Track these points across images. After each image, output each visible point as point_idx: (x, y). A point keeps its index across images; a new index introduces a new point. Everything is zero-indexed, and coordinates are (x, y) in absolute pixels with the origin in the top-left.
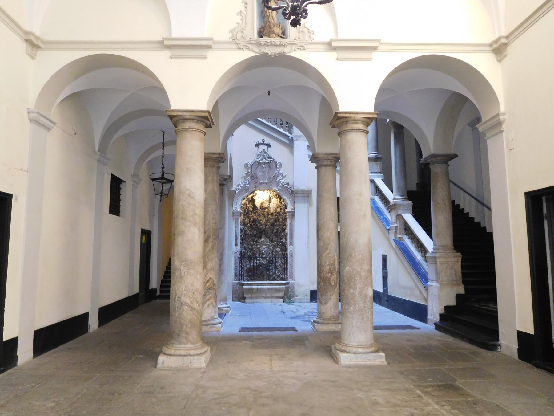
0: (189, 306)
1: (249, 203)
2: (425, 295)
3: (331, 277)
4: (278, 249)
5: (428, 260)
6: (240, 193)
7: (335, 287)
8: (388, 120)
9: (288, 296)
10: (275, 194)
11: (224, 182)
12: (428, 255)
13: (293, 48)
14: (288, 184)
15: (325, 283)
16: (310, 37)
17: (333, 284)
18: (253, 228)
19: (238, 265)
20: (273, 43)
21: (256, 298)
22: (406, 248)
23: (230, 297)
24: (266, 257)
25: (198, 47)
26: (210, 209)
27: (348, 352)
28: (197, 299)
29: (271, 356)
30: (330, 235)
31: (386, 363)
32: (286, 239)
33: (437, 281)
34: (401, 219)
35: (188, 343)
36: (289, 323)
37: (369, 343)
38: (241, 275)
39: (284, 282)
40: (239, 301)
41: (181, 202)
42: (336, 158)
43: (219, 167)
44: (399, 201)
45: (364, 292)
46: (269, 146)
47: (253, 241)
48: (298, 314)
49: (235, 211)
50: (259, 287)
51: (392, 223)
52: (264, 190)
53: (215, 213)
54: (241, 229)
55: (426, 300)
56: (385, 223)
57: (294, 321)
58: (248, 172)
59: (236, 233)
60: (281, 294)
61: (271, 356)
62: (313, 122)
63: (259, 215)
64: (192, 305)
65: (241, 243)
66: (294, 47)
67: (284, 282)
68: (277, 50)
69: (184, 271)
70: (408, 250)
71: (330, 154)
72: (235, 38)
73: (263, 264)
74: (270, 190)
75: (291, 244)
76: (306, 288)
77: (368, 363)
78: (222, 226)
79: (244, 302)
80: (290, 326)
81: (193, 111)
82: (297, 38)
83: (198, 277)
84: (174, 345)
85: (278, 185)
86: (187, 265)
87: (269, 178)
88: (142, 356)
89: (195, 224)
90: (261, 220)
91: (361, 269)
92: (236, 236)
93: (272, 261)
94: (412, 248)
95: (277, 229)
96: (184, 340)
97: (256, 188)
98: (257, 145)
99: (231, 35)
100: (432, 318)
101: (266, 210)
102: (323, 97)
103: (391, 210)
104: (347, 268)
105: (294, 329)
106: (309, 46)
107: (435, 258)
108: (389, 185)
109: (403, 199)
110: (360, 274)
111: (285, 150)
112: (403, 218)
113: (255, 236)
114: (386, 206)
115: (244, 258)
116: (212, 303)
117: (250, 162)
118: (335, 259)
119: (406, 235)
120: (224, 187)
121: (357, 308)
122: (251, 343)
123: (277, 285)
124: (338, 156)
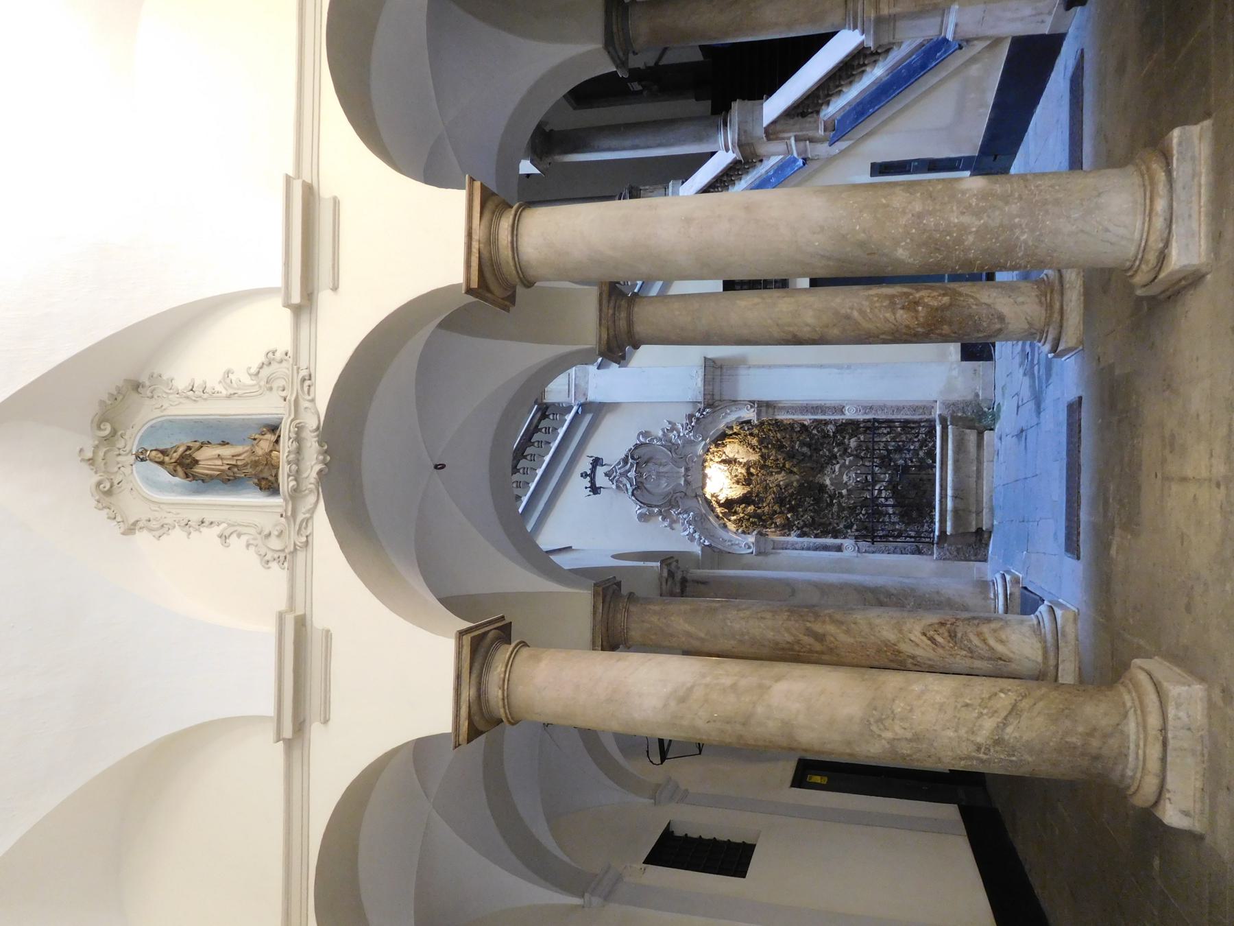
0: (1005, 723)
1: (736, 513)
2: (980, 46)
3: (926, 305)
4: (853, 443)
5: (885, 40)
6: (710, 536)
7: (955, 294)
8: (526, 167)
9: (976, 419)
10: (713, 449)
11: (679, 579)
12: (870, 44)
13: (307, 404)
14: (690, 417)
15: (943, 321)
16: (281, 362)
17: (946, 299)
18: (799, 505)
19: (891, 546)
20: (292, 457)
21: (979, 502)
22: (854, 109)
23: (975, 568)
24: (873, 474)
25: (309, 216)
26: (737, 626)
27: (1167, 244)
28: (986, 695)
29: (1167, 479)
30: (807, 307)
31: (1207, 123)
32: (826, 423)
33: (943, 11)
34: (779, 127)
35: (1122, 732)
36: (1054, 421)
37: (1137, 180)
38: (918, 537)
39: (938, 428)
40: (987, 545)
41: (700, 723)
42: (610, 296)
43: (631, 595)
44: (731, 135)
45: (974, 201)
46: (597, 462)
47: (832, 504)
48: (1026, 393)
49: (753, 549)
50: (950, 492)
51: (789, 151)
52: (705, 476)
53: (748, 613)
54: (799, 536)
55: (996, 41)
56: (789, 171)
57: (1048, 402)
58: (660, 513)
59: (808, 549)
60: (972, 436)
61: (1167, 479)
62: (518, 357)
63: (766, 488)
64: (1004, 714)
65: (836, 537)
66: (304, 404)
67: (938, 428)
68: (312, 448)
69: (898, 729)
70: (858, 104)
71: (601, 310)
72: (282, 555)
73: (890, 482)
74: (705, 461)
75: (841, 410)
76: (955, 373)
77: (1203, 180)
78: (790, 588)
79: (990, 533)
80: (1063, 416)
81: (458, 677)
82: (284, 394)
83: (917, 688)
84: (1129, 773)
85: (691, 442)
86: (880, 721)
87: (675, 462)
88: (1157, 862)
89: (763, 689)
90: (778, 485)
91: (904, 212)
92: (816, 548)
93: (882, 458)
94: (852, 93)
95: (803, 444)
96: (1113, 742)
97: (699, 495)
98: (595, 490)
99: (274, 565)
100: (1049, 20)
101: (752, 470)
102: (440, 325)
103: (755, 155)
104: (901, 253)
105: (1074, 408)
106: (303, 364)
107: (879, 21)
108: (701, 160)
109: (725, 125)
110: (920, 216)
111: (609, 424)
112: (774, 122)
113: (818, 501)
114: (746, 172)
115: (874, 531)
116: (995, 631)
117: (635, 509)
118: (877, 295)
119: (818, 112)
120: (689, 577)
121: (1024, 221)
122: (1117, 531)
123: (945, 449)
124: (606, 289)
